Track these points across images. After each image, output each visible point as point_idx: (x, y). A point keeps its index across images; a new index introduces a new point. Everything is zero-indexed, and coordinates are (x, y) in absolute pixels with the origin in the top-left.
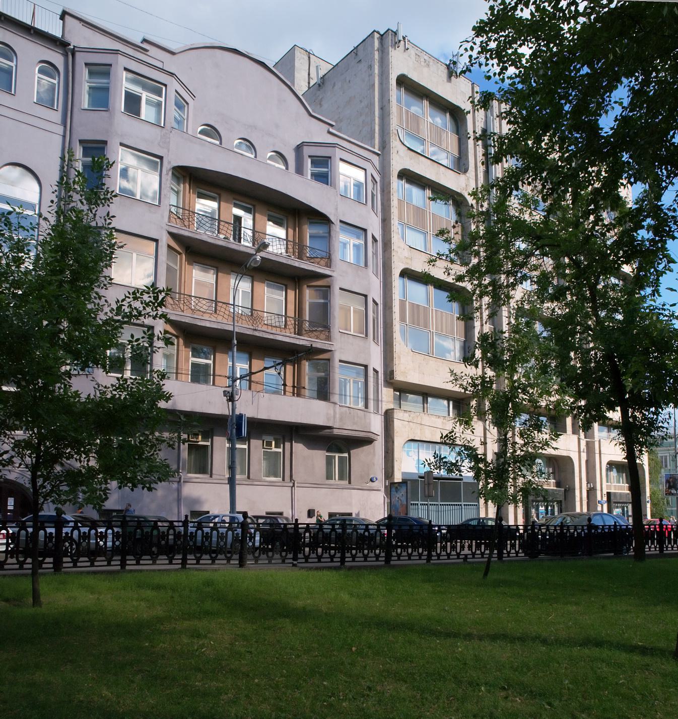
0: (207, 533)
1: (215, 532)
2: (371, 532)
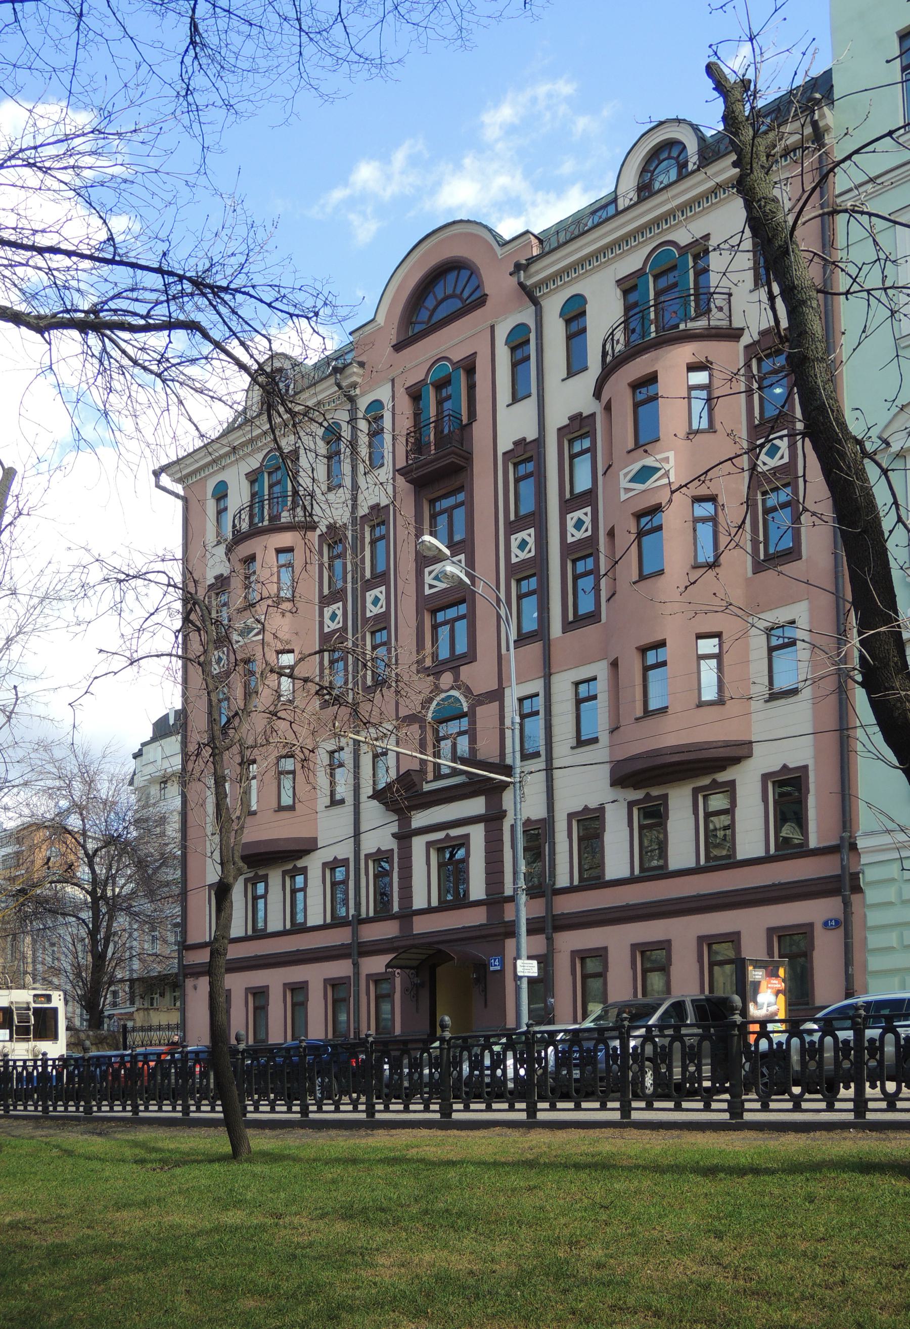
0: (692, 1047)
1: (677, 1045)
2: (776, 1037)
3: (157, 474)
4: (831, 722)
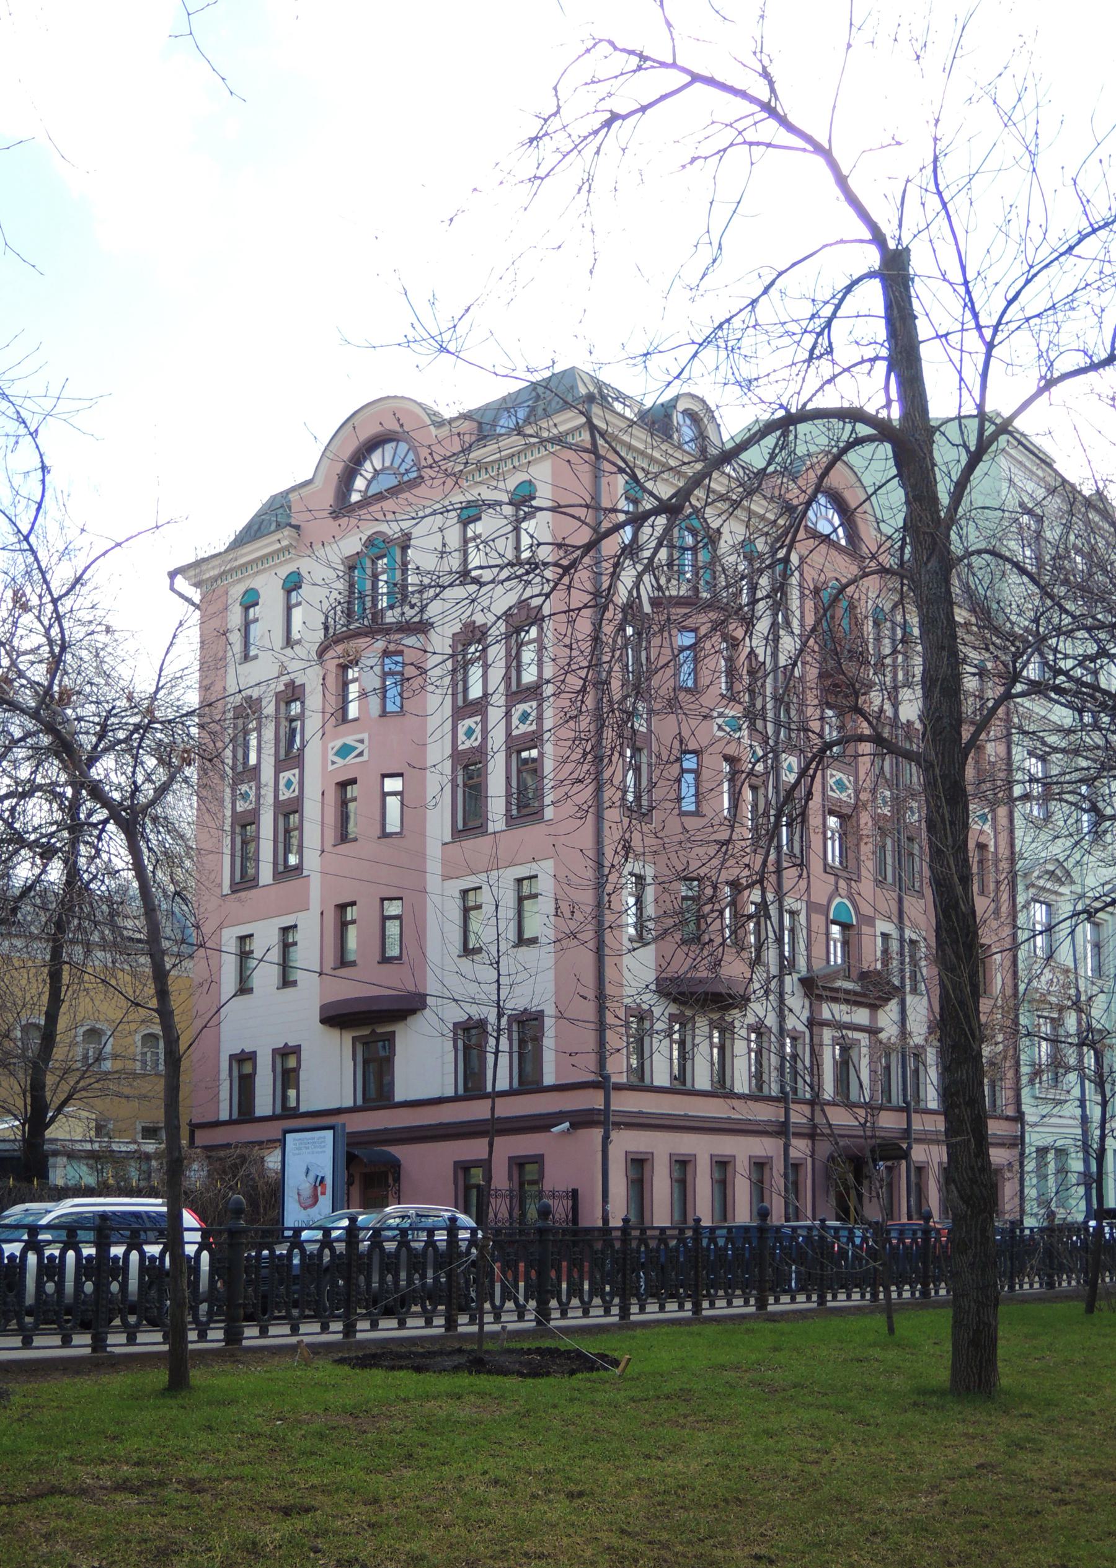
3: (172, 575)
4: (609, 961)
